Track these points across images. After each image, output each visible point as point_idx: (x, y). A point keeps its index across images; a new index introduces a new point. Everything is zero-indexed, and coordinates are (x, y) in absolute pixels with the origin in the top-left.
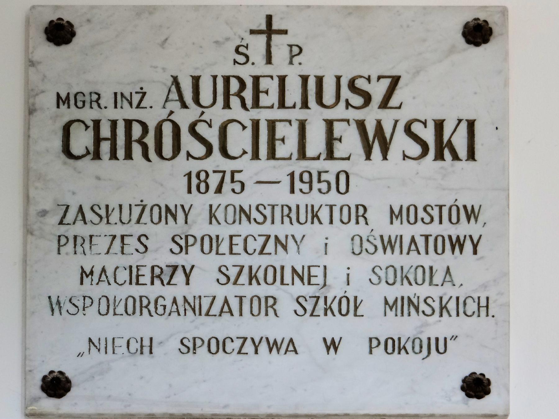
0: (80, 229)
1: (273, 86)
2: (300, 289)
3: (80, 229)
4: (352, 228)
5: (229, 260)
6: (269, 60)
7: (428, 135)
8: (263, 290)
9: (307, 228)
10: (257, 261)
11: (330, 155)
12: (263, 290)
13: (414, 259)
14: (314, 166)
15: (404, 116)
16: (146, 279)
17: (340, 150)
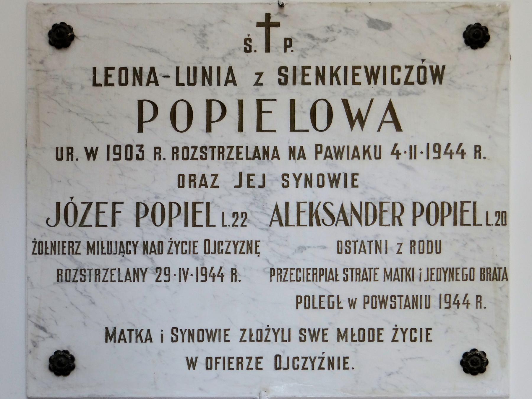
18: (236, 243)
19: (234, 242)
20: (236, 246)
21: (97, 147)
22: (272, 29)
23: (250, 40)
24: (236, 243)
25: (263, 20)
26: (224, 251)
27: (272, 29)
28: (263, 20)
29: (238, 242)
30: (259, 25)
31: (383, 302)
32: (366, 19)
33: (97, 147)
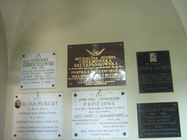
0: (24, 73)
1: (103, 104)
2: (40, 77)
3: (24, 73)
4: (44, 72)
5: (35, 75)
6: (39, 57)
7: (50, 63)
8: (37, 78)
9: (41, 72)
10: (37, 75)
11: (43, 66)
12: (37, 78)
13: (49, 74)
14: (42, 66)
15: (48, 62)
16: (116, 116)
17: (44, 65)
31: (50, 131)
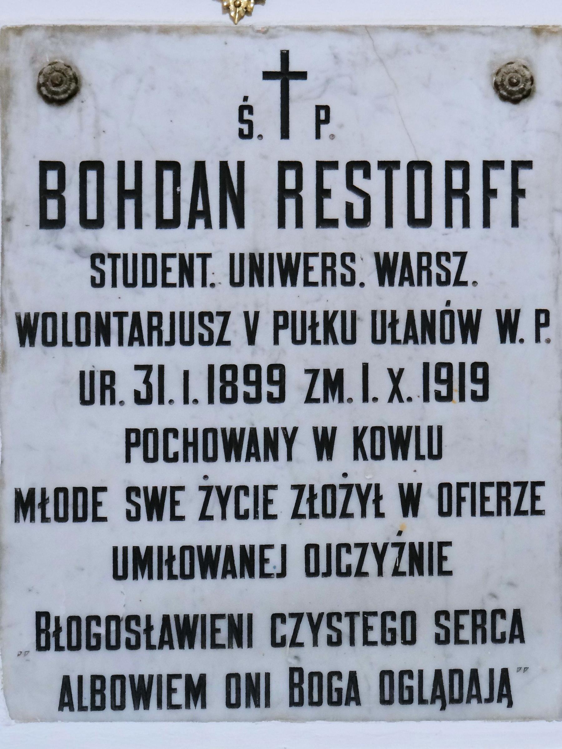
18: (380, 548)
19: (375, 546)
20: (380, 557)
21: (400, 369)
22: (294, 84)
23: (250, 109)
24: (380, 548)
25: (276, 67)
26: (354, 570)
27: (294, 84)
28: (276, 67)
29: (385, 546)
30: (268, 75)
32: (528, 31)
33: (400, 369)
